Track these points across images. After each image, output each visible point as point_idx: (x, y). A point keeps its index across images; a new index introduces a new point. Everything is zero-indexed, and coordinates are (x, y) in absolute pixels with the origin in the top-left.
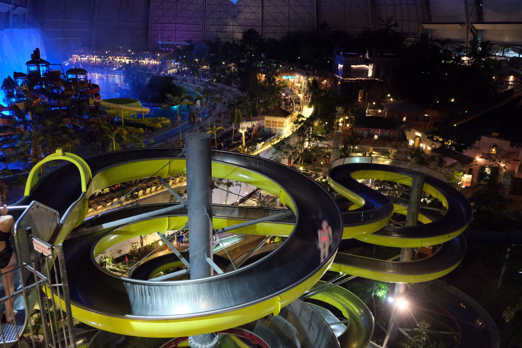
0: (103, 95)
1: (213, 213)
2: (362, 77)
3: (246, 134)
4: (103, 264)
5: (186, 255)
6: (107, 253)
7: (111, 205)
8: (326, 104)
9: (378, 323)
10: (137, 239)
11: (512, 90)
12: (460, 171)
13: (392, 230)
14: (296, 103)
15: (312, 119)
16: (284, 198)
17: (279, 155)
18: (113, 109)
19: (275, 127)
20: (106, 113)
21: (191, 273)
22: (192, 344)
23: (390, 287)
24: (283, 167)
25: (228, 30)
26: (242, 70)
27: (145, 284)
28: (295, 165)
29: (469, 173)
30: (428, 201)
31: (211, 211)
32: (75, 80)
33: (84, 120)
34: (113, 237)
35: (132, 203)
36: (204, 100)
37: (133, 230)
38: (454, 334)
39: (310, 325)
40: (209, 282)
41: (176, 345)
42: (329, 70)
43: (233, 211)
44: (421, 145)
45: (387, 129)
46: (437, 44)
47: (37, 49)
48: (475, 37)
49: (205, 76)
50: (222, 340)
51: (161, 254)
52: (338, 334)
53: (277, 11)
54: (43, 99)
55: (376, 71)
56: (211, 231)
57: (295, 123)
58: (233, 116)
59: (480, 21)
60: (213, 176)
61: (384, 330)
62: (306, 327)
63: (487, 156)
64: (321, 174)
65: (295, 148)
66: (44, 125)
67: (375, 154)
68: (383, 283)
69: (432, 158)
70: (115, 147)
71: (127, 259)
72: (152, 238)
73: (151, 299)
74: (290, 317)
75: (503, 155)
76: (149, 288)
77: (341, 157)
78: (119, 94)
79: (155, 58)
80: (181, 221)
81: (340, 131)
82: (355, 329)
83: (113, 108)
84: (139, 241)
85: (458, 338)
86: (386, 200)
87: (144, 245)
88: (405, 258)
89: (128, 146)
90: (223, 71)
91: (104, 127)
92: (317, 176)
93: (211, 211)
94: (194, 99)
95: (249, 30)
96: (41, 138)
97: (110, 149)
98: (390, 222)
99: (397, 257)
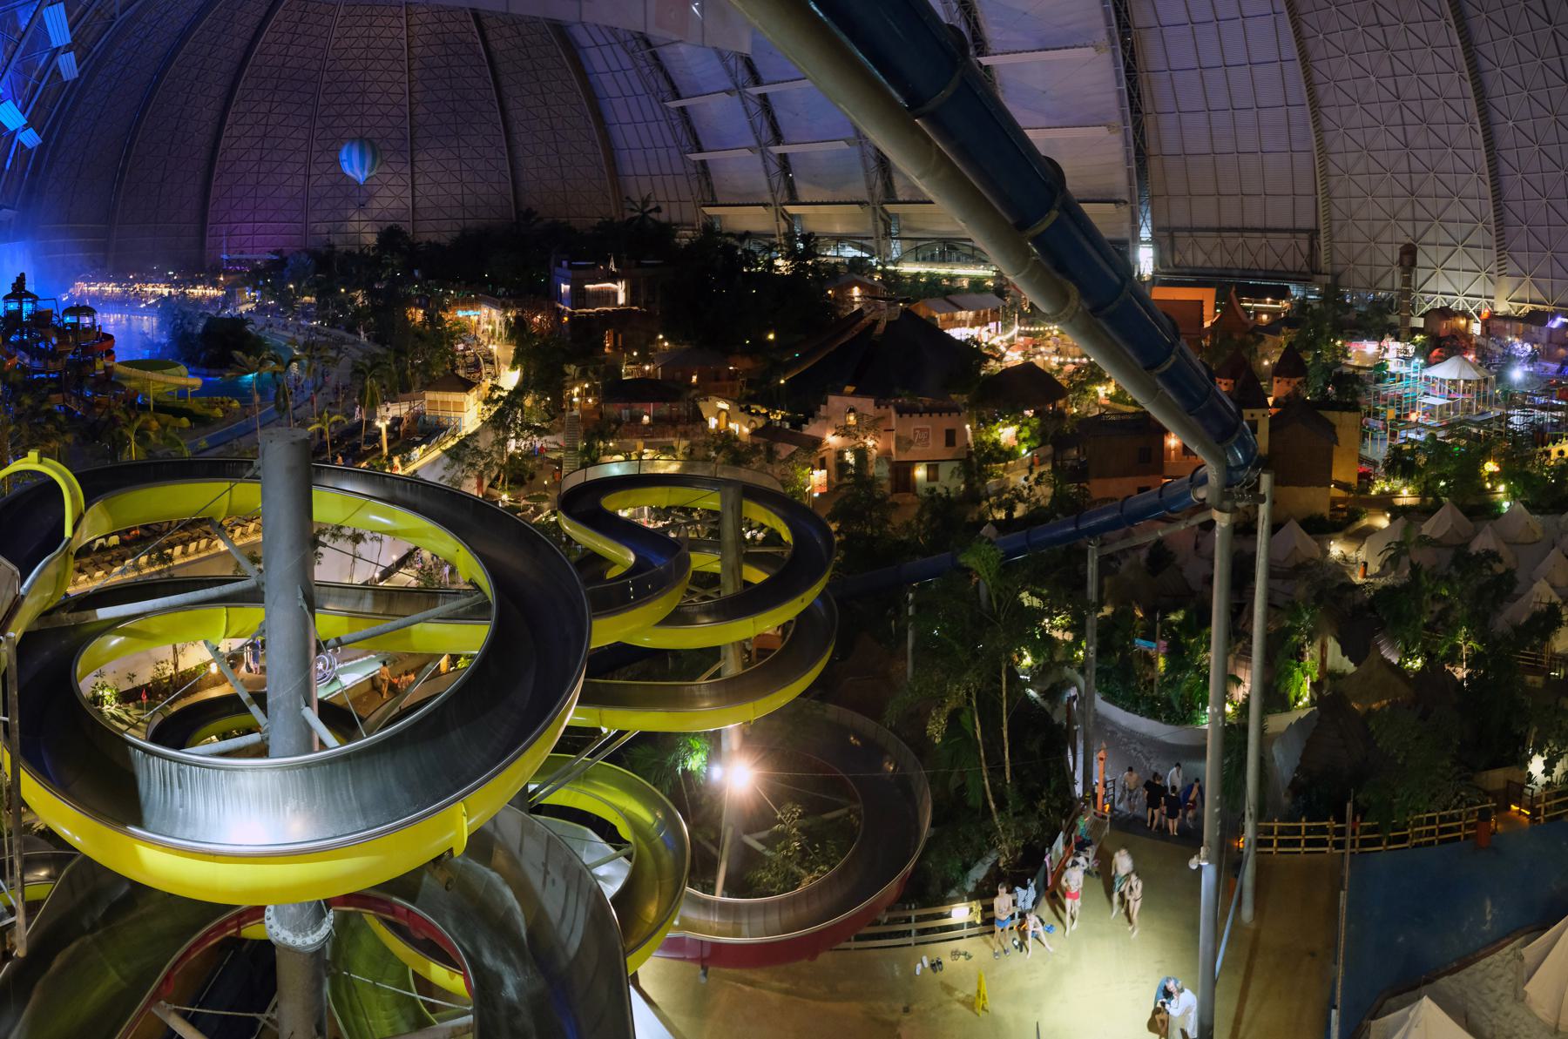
0: (121, 355)
1: (317, 603)
2: (607, 304)
3: (389, 429)
4: (97, 700)
5: (260, 699)
6: (106, 674)
7: (122, 572)
8: (545, 362)
9: (699, 837)
10: (165, 651)
11: (860, 310)
12: (805, 465)
13: (696, 609)
14: (486, 362)
15: (518, 392)
16: (469, 567)
17: (457, 472)
18: (137, 380)
19: (447, 414)
20: (122, 387)
21: (270, 743)
22: (273, 931)
23: (710, 743)
24: (466, 499)
25: (351, 229)
26: (383, 305)
27: (171, 759)
28: (493, 491)
29: (822, 467)
30: (760, 536)
31: (312, 598)
32: (75, 326)
33: (84, 399)
34: (115, 641)
35: (159, 572)
36: (305, 362)
37: (156, 630)
38: (851, 811)
39: (546, 873)
40: (307, 766)
41: (239, 931)
42: (545, 296)
43: (361, 598)
44: (731, 425)
45: (665, 401)
46: (730, 240)
47: (23, 274)
48: (791, 226)
49: (309, 317)
50: (342, 923)
51: (214, 693)
52: (610, 890)
53: (441, 192)
54: (22, 359)
55: (632, 293)
56: (313, 645)
57: (486, 402)
58: (362, 393)
59: (794, 200)
60: (316, 517)
61: (714, 850)
62: (536, 879)
63: (844, 431)
64: (546, 505)
65: (489, 454)
66: (19, 404)
67: (649, 454)
68: (697, 734)
69: (754, 449)
70: (133, 452)
71: (144, 697)
72: (195, 656)
73: (182, 796)
74: (500, 858)
75: (873, 425)
76: (179, 770)
77: (584, 466)
78: (147, 352)
79: (215, 284)
80: (252, 616)
81: (576, 412)
82: (650, 865)
83: (135, 379)
84: (171, 659)
85: (859, 817)
86: (675, 546)
87: (181, 669)
88: (731, 667)
89: (159, 453)
90: (341, 306)
91: (116, 413)
92: (538, 511)
93: (312, 598)
94: (286, 360)
95: (390, 228)
96: (12, 428)
97: (125, 457)
98: (691, 593)
99: (716, 668)
